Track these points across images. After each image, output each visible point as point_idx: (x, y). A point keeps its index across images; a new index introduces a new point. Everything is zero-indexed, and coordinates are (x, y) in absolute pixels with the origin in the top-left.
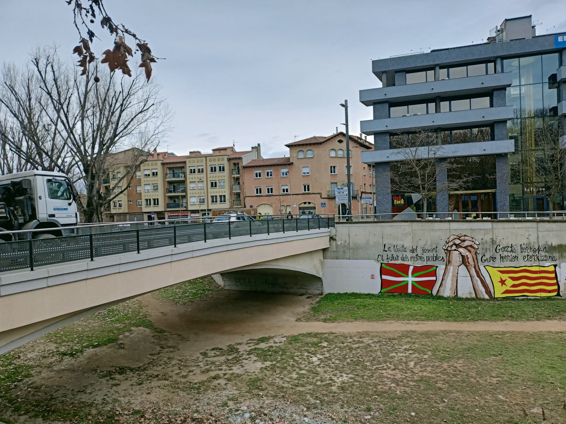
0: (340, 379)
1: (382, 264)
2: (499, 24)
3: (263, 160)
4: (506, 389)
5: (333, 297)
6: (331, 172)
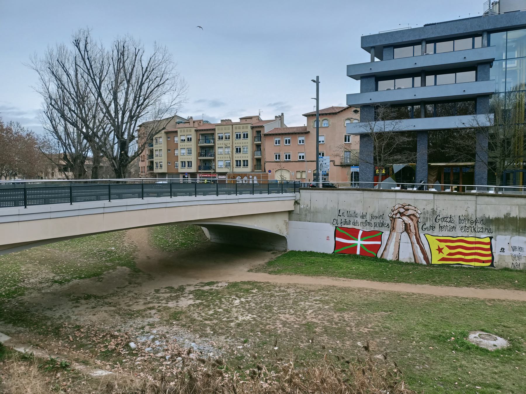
1: (336, 227)
3: (287, 128)
6: (346, 141)
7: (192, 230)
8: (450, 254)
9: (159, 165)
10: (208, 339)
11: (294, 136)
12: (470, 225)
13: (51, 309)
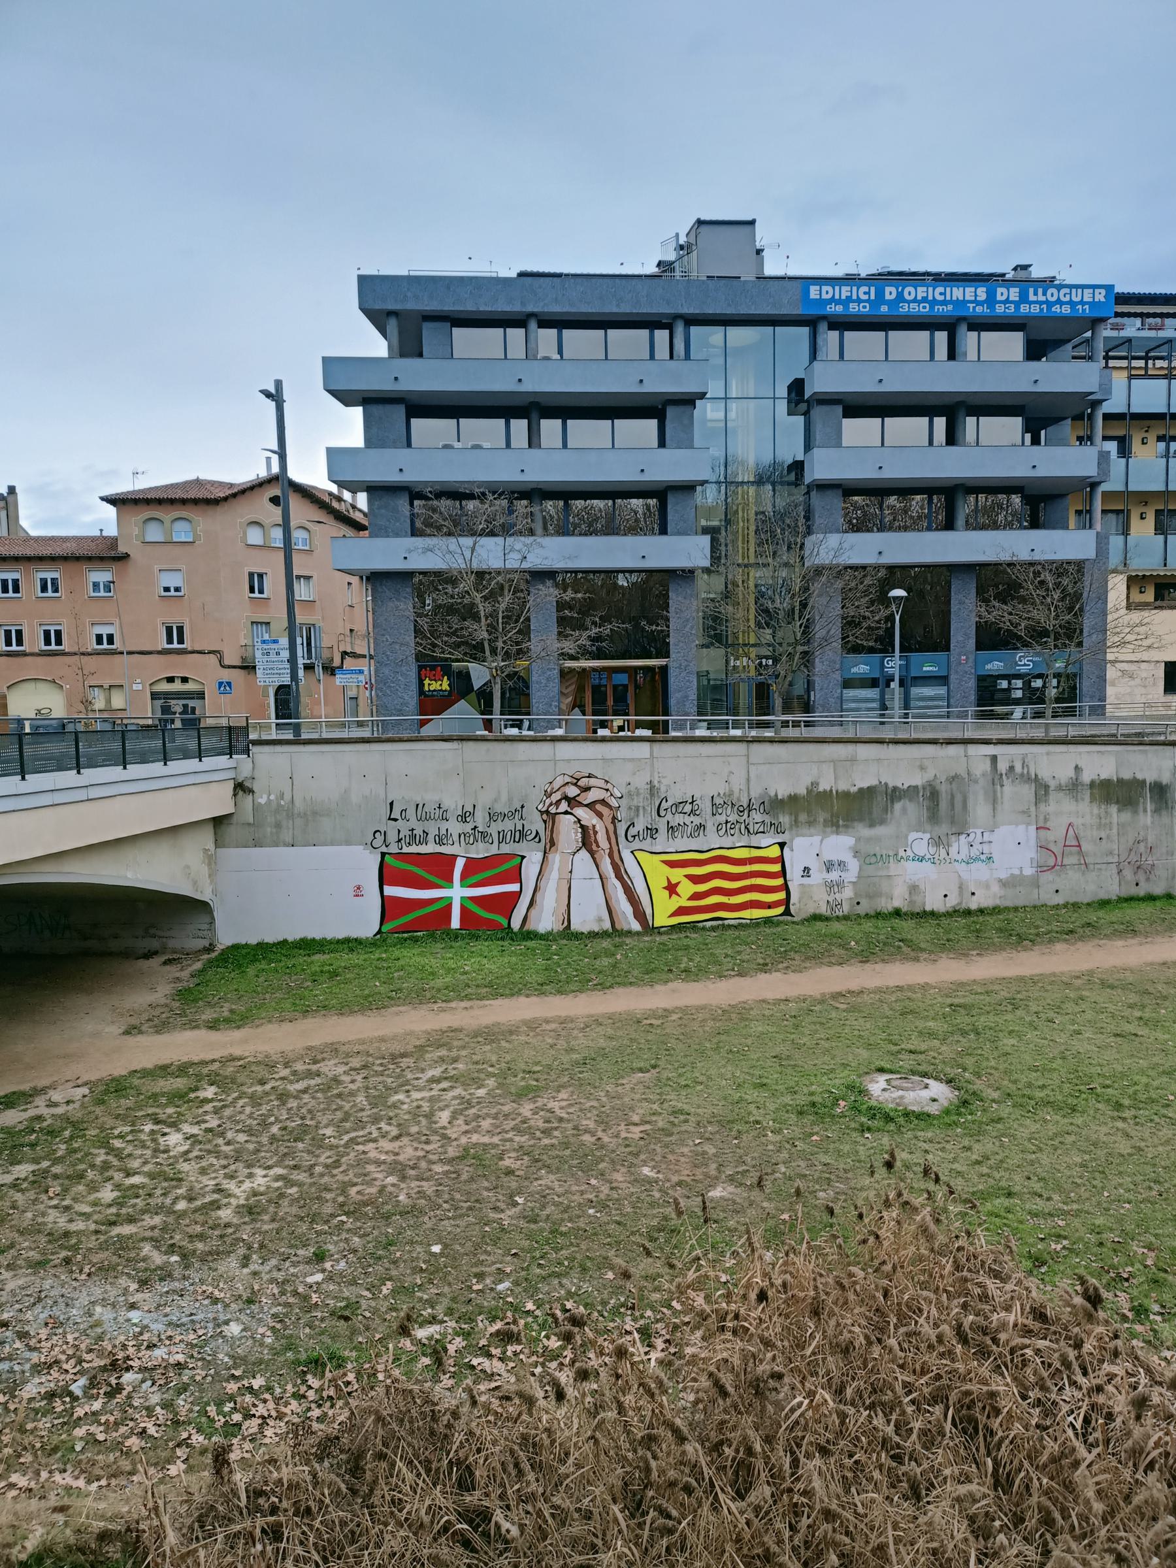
0: (247, 1185)
1: (383, 855)
2: (683, 229)
3: (28, 539)
4: (659, 1150)
5: (244, 957)
6: (252, 590)
8: (696, 896)
11: (72, 566)
12: (736, 817)
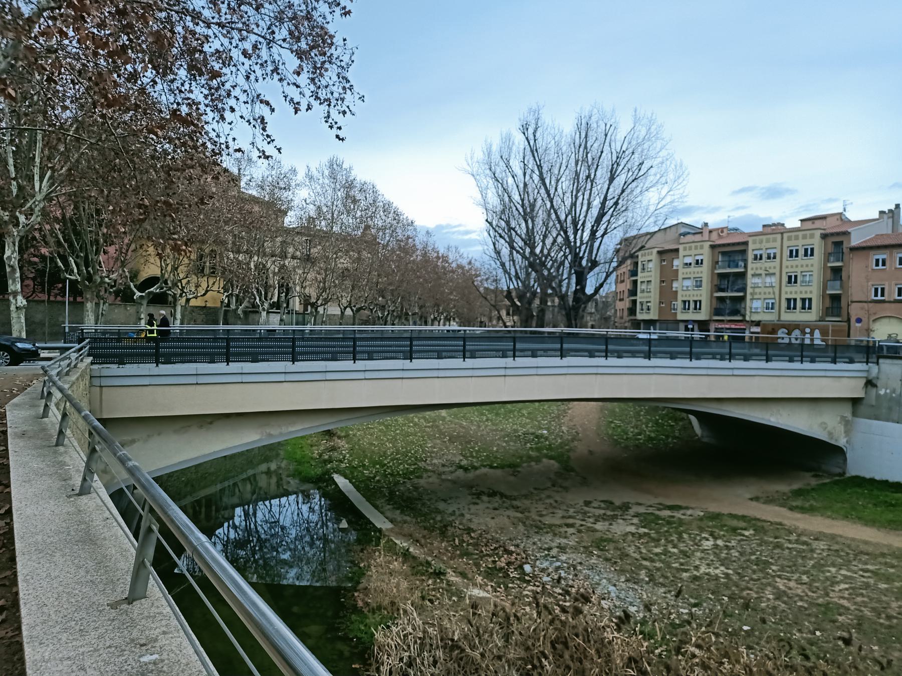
7: (671, 419)
9: (645, 307)
10: (636, 587)
13: (445, 501)
